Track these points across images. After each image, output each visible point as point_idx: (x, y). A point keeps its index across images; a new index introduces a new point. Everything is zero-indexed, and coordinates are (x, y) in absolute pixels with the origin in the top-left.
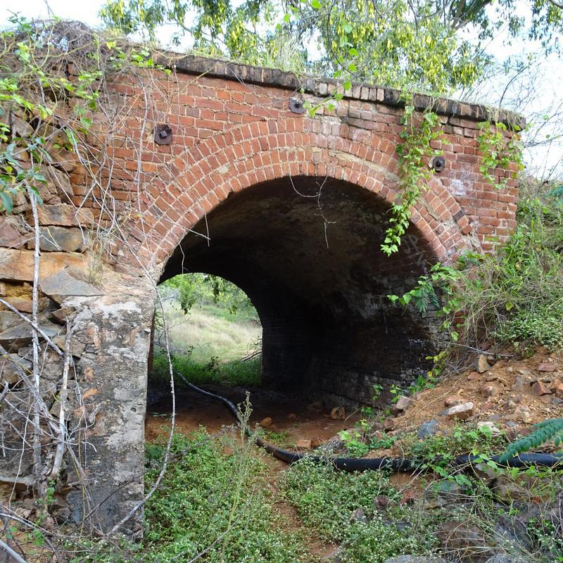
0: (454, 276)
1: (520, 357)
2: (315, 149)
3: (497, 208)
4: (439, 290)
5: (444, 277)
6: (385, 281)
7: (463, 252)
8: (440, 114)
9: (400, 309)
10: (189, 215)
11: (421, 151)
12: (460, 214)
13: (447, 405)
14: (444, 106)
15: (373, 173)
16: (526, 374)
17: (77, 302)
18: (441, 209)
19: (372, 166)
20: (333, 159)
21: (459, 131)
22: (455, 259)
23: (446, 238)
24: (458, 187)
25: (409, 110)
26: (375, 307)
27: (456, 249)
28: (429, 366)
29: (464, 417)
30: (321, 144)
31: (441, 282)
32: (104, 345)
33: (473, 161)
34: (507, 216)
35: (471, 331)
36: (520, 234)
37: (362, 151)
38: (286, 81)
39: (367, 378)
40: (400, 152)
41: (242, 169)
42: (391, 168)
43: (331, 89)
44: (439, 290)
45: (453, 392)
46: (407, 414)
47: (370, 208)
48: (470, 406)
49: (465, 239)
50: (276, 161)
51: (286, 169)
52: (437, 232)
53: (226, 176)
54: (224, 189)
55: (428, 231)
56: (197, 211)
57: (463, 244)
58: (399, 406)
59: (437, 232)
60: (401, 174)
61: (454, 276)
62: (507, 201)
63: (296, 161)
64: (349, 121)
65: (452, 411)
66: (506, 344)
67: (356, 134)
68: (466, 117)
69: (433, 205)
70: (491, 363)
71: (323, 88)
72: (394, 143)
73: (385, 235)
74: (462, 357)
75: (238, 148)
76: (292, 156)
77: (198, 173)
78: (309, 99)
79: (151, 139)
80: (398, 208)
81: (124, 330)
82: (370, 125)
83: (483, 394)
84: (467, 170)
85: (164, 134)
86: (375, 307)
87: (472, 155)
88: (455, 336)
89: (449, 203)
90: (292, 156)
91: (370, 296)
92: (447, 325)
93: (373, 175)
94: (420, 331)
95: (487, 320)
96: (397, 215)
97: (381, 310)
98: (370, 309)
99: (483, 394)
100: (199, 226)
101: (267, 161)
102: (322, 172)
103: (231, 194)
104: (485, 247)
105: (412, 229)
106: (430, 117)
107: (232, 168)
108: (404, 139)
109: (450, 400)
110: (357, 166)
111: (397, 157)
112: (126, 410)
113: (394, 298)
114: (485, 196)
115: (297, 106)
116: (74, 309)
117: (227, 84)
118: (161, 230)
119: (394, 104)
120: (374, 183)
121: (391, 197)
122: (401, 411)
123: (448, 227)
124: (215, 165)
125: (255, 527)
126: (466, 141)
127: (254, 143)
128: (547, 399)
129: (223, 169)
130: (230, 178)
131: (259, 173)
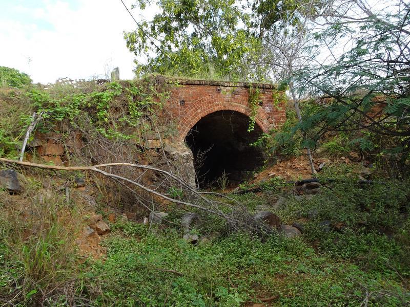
0: (269, 137)
1: (288, 160)
2: (225, 102)
3: (280, 115)
4: (264, 141)
5: (265, 137)
6: (246, 138)
7: (271, 129)
8: (261, 88)
9: (253, 147)
10: (191, 125)
11: (256, 101)
12: (269, 118)
13: (269, 174)
14: (262, 86)
15: (242, 107)
16: (289, 164)
17: (174, 153)
18: (263, 116)
19: (242, 105)
20: (230, 104)
21: (267, 93)
22: (269, 131)
23: (265, 125)
24: (268, 109)
25: (251, 89)
26: (244, 147)
27: (268, 128)
28: (263, 164)
29: (273, 176)
30: (227, 100)
31: (265, 139)
32: (184, 163)
33: (272, 101)
34: (283, 117)
35: (275, 153)
36: (288, 122)
37: (239, 101)
38: (215, 83)
39: (242, 172)
40: (250, 101)
41: (204, 110)
42: (247, 105)
43: (228, 85)
44: (264, 141)
45: (270, 171)
46: (258, 178)
47: (241, 119)
48: (274, 173)
49: (271, 125)
50: (214, 107)
51: (216, 109)
52: (262, 124)
53: (200, 113)
54: (200, 116)
55: (260, 124)
56: (193, 124)
57: (270, 126)
58: (255, 176)
59: (262, 124)
60: (250, 107)
61: (269, 137)
62: (283, 112)
63: (219, 106)
64: (234, 93)
65: (270, 175)
66: (284, 156)
67: (236, 96)
68: (268, 88)
69: (261, 116)
70: (280, 162)
71: (226, 84)
72: (248, 98)
73: (249, 126)
74: (272, 161)
75: (203, 104)
76: (218, 105)
77: (192, 113)
78: (222, 88)
79: (179, 104)
80: (251, 118)
81: (187, 159)
82: (240, 93)
83: (278, 170)
84: (270, 104)
85: (183, 102)
86: (244, 147)
87: (271, 100)
88: (270, 155)
89: (265, 114)
90: (218, 105)
91: (241, 143)
92: (267, 152)
93: (242, 109)
94: (260, 154)
95: (279, 149)
96: (251, 120)
97: (246, 148)
98: (242, 147)
99: (278, 170)
100: (194, 128)
101: (211, 107)
102: (227, 109)
103: (202, 117)
104: (277, 127)
105: (256, 124)
106: (257, 90)
107: (202, 110)
108: (251, 97)
109: (269, 173)
110: (237, 106)
111: (248, 102)
112: (191, 178)
113: (251, 144)
114: (277, 111)
115: (219, 90)
116: (174, 155)
117: (199, 86)
118: (184, 130)
119: (246, 87)
120: (243, 111)
121: (248, 114)
122: (256, 178)
123: (265, 122)
124: (197, 110)
125: (307, 58)
126: (269, 95)
127: (207, 102)
128: (294, 170)
129: (199, 111)
130: (202, 113)
131: (210, 111)
